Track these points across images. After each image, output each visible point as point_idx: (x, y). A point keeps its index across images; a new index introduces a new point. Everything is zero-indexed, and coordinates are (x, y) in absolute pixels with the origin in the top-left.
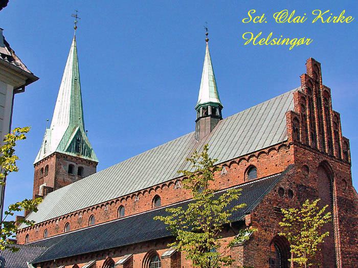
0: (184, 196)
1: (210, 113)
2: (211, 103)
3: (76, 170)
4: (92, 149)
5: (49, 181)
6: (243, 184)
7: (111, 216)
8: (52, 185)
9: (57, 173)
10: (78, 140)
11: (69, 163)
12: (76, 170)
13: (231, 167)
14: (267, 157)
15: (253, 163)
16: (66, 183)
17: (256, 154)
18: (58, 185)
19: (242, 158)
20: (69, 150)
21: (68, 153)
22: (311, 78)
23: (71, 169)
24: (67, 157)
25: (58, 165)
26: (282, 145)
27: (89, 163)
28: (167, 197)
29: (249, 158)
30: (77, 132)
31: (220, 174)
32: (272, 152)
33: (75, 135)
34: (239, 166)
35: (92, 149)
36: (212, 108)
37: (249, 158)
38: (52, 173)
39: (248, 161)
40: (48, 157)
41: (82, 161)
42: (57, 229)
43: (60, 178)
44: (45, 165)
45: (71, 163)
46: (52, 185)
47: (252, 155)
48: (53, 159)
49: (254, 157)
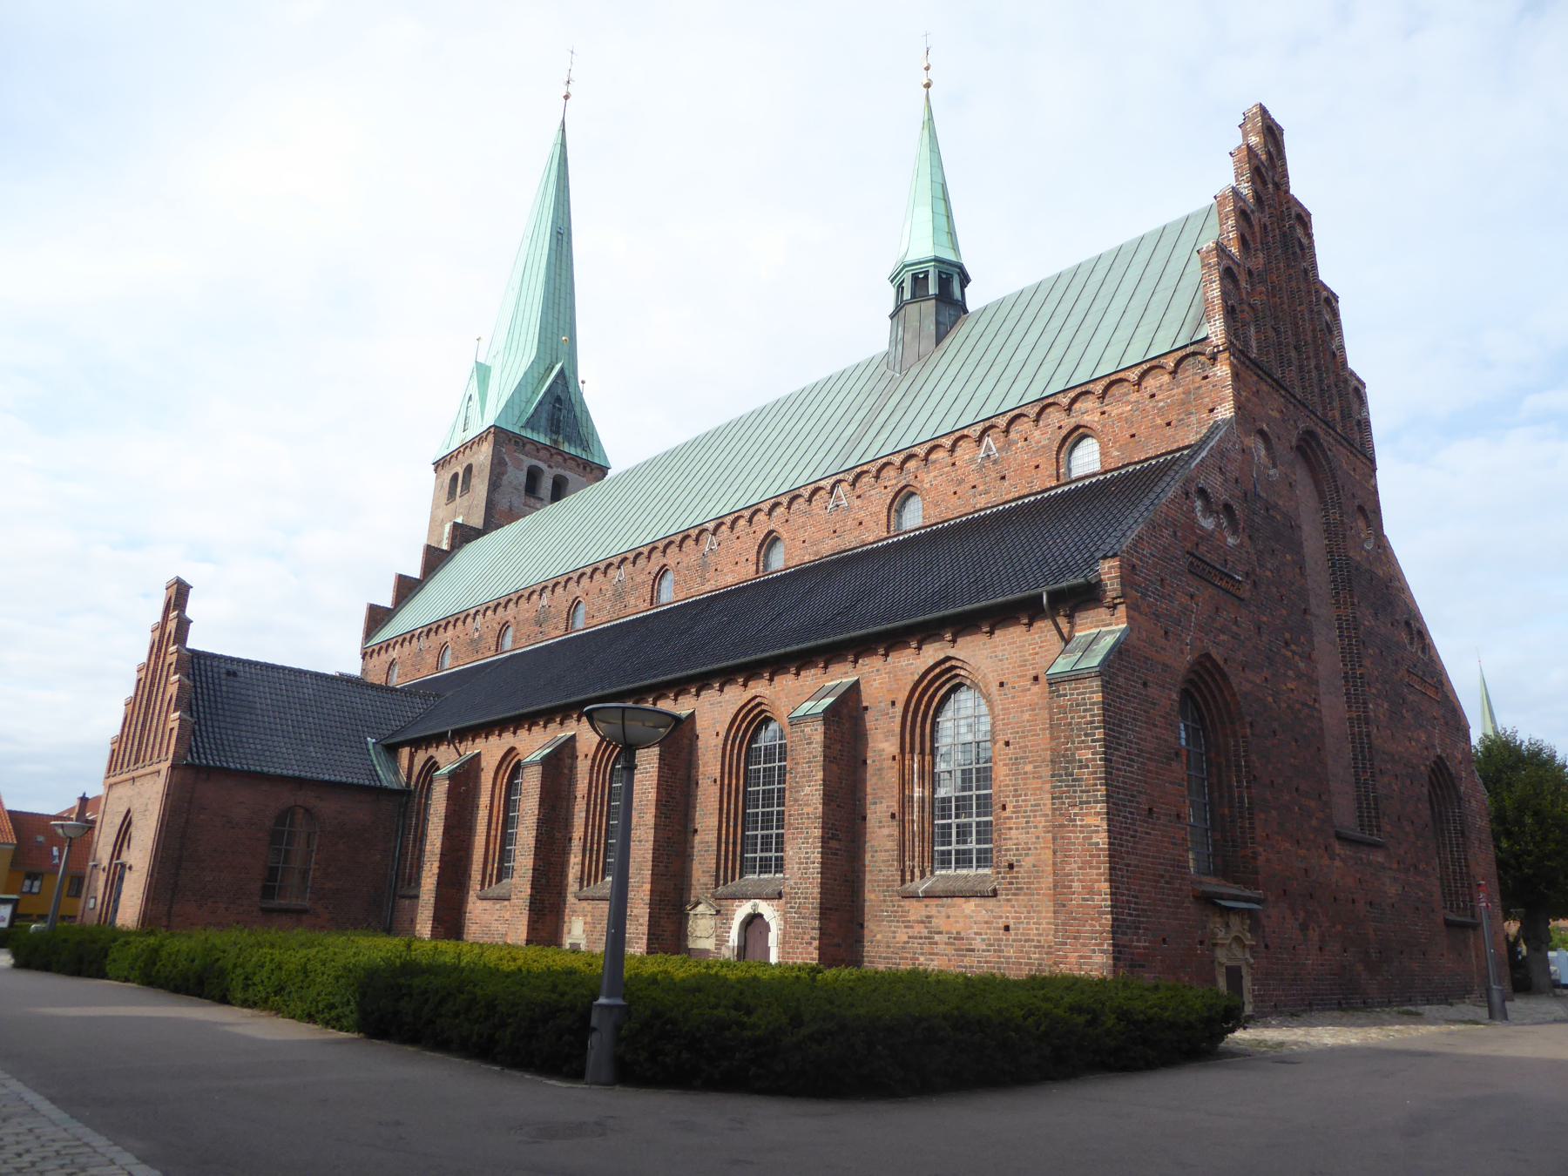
0: (857, 533)
1: (933, 289)
2: (937, 260)
3: (546, 485)
4: (594, 1029)
5: (471, 509)
6: (886, 538)
7: (632, 602)
8: (477, 521)
9: (494, 486)
10: (558, 400)
11: (529, 462)
12: (546, 485)
13: (1013, 435)
14: (1134, 397)
15: (1086, 419)
16: (512, 516)
17: (1099, 388)
18: (495, 518)
19: (1045, 405)
20: (531, 424)
21: (529, 434)
22: (1262, 163)
23: (533, 476)
24: (524, 445)
25: (498, 467)
26: (1190, 354)
27: (585, 468)
28: (802, 535)
29: (1074, 401)
30: (557, 376)
31: (972, 461)
32: (1151, 383)
33: (551, 386)
34: (1037, 434)
35: (594, 1029)
36: (940, 276)
37: (1074, 401)
38: (480, 487)
39: (1069, 409)
40: (473, 442)
41: (565, 460)
42: (474, 644)
43: (503, 504)
44: (465, 465)
45: (535, 462)
46: (477, 521)
47: (1082, 392)
48: (486, 449)
49: (1126, 384)
